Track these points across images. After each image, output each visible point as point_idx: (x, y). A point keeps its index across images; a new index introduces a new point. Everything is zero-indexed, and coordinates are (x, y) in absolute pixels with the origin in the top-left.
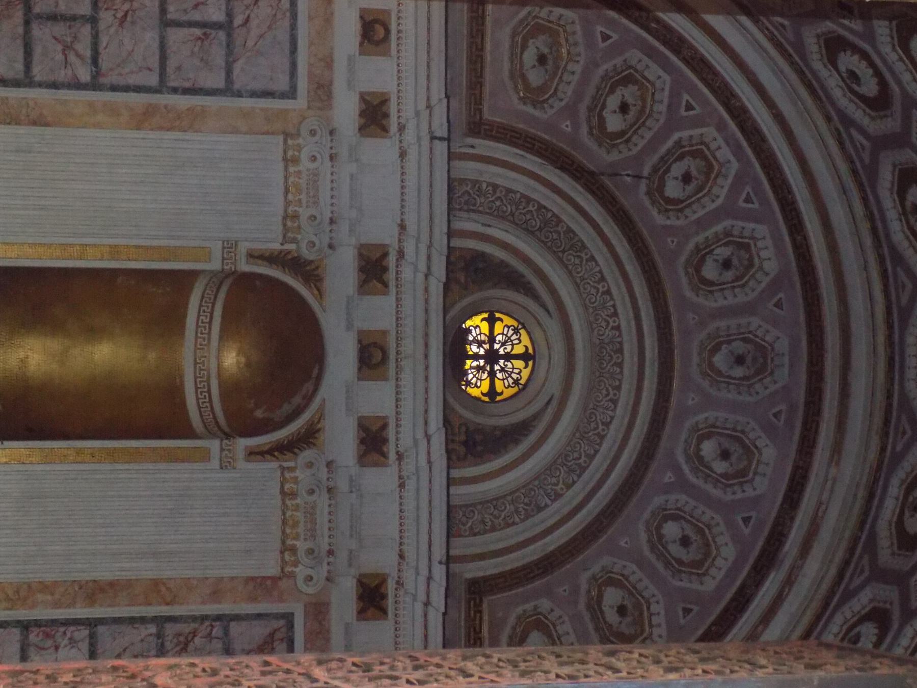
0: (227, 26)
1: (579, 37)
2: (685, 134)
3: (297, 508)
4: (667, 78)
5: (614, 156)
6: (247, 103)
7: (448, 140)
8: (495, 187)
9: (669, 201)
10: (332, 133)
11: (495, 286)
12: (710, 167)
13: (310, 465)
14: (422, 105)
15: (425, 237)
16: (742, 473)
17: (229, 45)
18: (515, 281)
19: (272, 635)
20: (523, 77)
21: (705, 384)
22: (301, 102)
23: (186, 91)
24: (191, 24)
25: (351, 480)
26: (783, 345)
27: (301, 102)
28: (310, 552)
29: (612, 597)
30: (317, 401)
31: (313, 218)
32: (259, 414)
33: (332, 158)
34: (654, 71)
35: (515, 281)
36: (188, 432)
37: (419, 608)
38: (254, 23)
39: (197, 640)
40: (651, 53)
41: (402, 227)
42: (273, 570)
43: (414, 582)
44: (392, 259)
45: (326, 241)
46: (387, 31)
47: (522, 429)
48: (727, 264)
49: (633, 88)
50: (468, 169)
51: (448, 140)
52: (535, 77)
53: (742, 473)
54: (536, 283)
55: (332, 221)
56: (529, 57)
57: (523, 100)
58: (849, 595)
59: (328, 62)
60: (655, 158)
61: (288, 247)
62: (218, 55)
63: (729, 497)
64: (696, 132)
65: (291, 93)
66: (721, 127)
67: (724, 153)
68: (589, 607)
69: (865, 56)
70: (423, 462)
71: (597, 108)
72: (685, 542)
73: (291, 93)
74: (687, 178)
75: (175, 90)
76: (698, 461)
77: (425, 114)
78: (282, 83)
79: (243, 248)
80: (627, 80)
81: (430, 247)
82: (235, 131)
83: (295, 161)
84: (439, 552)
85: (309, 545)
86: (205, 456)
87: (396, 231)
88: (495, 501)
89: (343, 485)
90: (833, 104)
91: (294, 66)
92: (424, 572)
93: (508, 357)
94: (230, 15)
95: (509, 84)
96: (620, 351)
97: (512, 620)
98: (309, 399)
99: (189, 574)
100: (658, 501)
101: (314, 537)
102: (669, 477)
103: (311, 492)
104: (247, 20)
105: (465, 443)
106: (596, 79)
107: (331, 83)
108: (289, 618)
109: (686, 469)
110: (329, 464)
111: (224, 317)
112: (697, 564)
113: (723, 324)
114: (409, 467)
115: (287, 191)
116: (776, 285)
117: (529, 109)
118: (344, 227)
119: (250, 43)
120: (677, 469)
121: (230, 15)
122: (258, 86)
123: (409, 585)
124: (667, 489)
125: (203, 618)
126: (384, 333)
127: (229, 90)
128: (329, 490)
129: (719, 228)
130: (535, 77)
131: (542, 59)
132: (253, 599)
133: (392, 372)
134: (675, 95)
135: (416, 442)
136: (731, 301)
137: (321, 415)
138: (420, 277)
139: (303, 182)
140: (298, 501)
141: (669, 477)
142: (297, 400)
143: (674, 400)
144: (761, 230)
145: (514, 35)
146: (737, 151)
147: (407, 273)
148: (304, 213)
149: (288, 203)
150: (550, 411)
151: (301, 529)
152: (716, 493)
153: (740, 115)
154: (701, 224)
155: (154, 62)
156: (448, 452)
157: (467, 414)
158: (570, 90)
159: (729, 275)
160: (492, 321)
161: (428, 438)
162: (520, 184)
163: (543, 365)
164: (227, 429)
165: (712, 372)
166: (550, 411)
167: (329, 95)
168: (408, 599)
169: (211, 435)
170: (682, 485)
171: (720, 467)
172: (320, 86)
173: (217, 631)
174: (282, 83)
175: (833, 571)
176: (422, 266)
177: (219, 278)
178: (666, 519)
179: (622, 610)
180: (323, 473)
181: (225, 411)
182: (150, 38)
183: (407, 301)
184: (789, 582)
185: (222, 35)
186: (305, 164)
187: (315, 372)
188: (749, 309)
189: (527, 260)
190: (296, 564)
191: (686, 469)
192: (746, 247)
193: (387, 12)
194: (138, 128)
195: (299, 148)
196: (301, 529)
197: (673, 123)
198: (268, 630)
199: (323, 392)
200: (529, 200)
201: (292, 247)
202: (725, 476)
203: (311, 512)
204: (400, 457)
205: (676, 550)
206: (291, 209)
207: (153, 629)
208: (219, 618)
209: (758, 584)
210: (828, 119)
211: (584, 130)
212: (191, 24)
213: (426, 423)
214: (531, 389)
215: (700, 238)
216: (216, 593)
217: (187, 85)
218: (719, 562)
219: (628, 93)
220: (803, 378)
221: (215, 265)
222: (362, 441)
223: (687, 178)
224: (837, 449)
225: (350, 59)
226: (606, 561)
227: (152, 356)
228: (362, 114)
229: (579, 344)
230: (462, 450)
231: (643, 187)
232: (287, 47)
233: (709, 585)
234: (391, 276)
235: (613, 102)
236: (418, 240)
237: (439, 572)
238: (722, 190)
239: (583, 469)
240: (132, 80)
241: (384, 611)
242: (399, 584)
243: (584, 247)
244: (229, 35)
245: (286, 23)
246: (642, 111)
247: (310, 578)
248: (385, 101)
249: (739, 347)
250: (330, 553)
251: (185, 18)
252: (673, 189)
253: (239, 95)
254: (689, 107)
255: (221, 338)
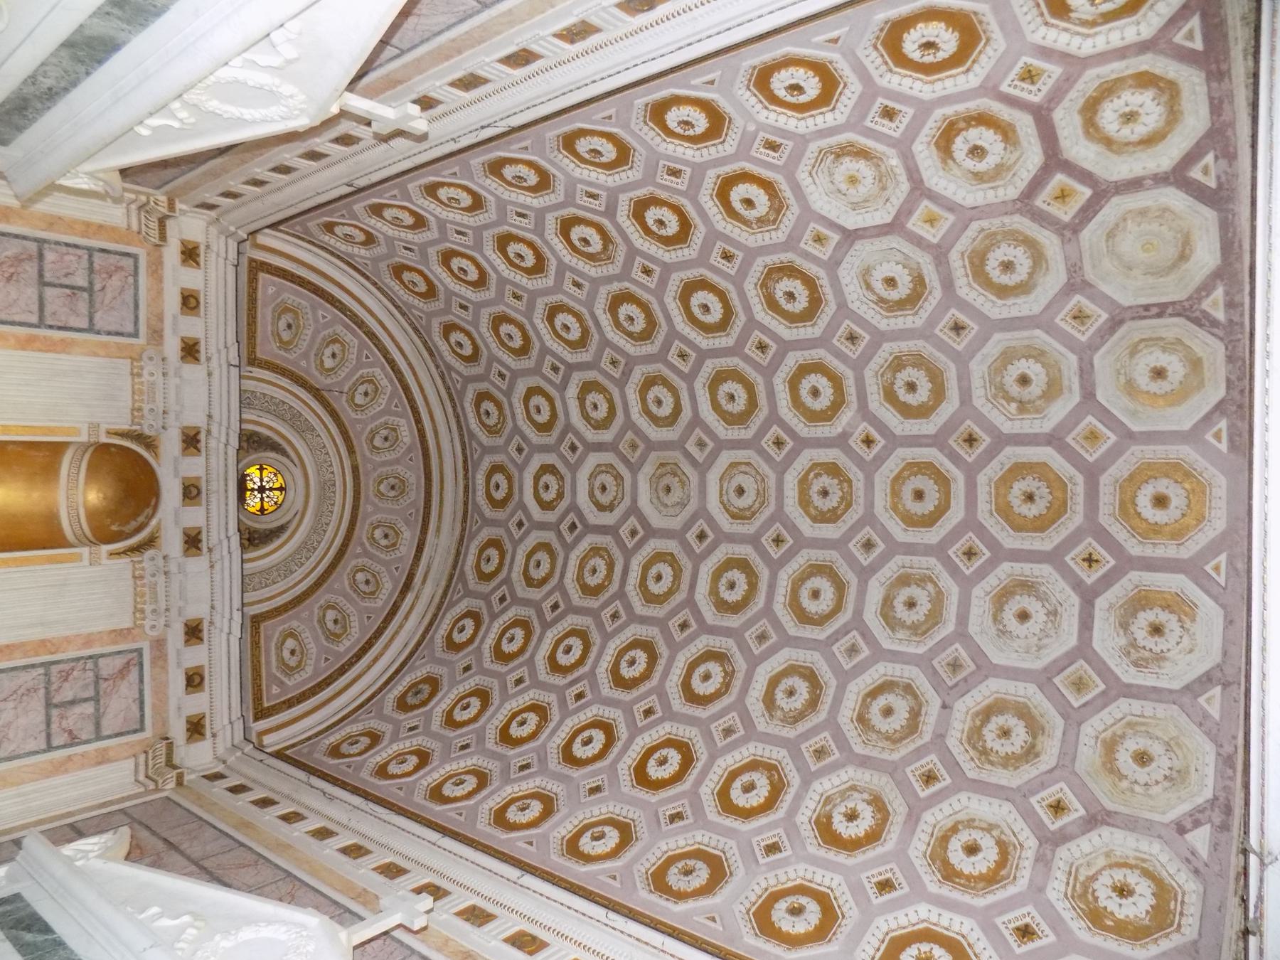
0: (90, 290)
1: (310, 316)
2: (365, 371)
3: (143, 586)
4: (356, 341)
5: (329, 381)
6: (104, 338)
7: (239, 366)
8: (265, 395)
9: (357, 405)
10: (163, 360)
11: (265, 450)
12: (377, 388)
13: (153, 559)
14: (221, 346)
15: (225, 423)
16: (394, 545)
17: (91, 303)
18: (275, 447)
19: (128, 663)
20: (278, 335)
21: (376, 501)
22: (141, 341)
23: (60, 328)
24: (62, 286)
25: (179, 565)
26: (413, 480)
27: (141, 341)
28: (154, 611)
29: (331, 615)
30: (154, 522)
31: (152, 410)
32: (114, 528)
33: (164, 374)
34: (349, 337)
35: (275, 447)
36: (63, 543)
37: (224, 637)
38: (109, 290)
39: (75, 673)
40: (347, 327)
41: (210, 416)
42: (127, 623)
43: (221, 622)
44: (202, 437)
45: (160, 424)
46: (198, 302)
47: (281, 529)
48: (386, 439)
49: (337, 345)
50: (249, 385)
51: (239, 366)
52: (286, 336)
53: (394, 545)
54: (292, 454)
55: (164, 412)
56: (282, 324)
57: (280, 348)
58: (452, 605)
59: (161, 318)
60: (351, 383)
61: (134, 428)
62: (83, 307)
63: (388, 558)
64: (370, 370)
65: (135, 335)
66: (383, 369)
67: (385, 382)
68: (319, 621)
69: (468, 334)
70: (225, 552)
71: (319, 355)
72: (367, 582)
73: (135, 335)
74: (366, 394)
75: (51, 327)
76: (372, 539)
77: (224, 352)
78: (129, 328)
79: (104, 427)
80: (335, 341)
81: (228, 428)
82: (96, 355)
83: (140, 375)
84: (237, 603)
85: (153, 607)
86: (79, 558)
87: (205, 419)
88: (267, 571)
89: (173, 568)
90: (442, 358)
91: (137, 317)
92: (227, 615)
93: (271, 489)
94: (91, 283)
95: (271, 338)
96: (334, 485)
97: (277, 635)
98: (150, 518)
99: (68, 633)
100: (354, 562)
101: (156, 602)
102: (359, 550)
103: (154, 575)
104: (103, 288)
105: (249, 540)
106: (319, 340)
107: (162, 330)
108: (139, 652)
109: (367, 545)
110: (165, 557)
111: (88, 470)
112: (373, 593)
113: (384, 469)
114: (216, 556)
115: (134, 393)
116: (409, 450)
117: (282, 353)
118: (172, 416)
119: (106, 302)
120: (362, 544)
121: (91, 283)
122: (113, 328)
123: (218, 624)
124: (358, 556)
125: (78, 659)
126: (198, 478)
127: (91, 329)
128: (166, 573)
129: (382, 420)
130: (286, 336)
131: (289, 326)
132: (115, 643)
133: (204, 502)
134: (360, 351)
135: (220, 541)
136: (389, 458)
137: (158, 528)
138: (222, 446)
139: (145, 388)
140: (145, 581)
141: (359, 550)
142: (141, 519)
143: (361, 509)
144: (403, 422)
145: (274, 311)
146: (391, 381)
147: (213, 443)
148: (146, 407)
149: (134, 401)
150: (298, 517)
151: (147, 598)
152: (383, 556)
153: (391, 362)
154: (374, 418)
155: (35, 308)
156: (242, 545)
157: (249, 523)
158: (305, 344)
159: (387, 444)
160: (261, 469)
161: (228, 538)
162: (279, 394)
163: (291, 493)
164: (92, 539)
165: (380, 495)
166: (298, 517)
167: (161, 337)
168: (217, 631)
169: (82, 544)
170: (366, 553)
171: (384, 542)
172: (155, 331)
173: (90, 665)
174: (129, 328)
175: (440, 591)
176: (223, 439)
177: (85, 447)
178: (357, 571)
179: (336, 622)
180: (160, 562)
181: (92, 529)
182: (31, 292)
183: (213, 460)
184: (417, 597)
185: (86, 295)
186: (146, 377)
187: (153, 503)
188: (397, 461)
189: (289, 442)
190: (144, 619)
191: (367, 545)
192: (395, 430)
193: (198, 292)
194: (23, 349)
195: (142, 368)
196: (147, 598)
197: (360, 365)
198: (125, 661)
199: (159, 515)
200: (284, 403)
201: (137, 427)
202: (387, 547)
203: (153, 587)
204: (210, 550)
205: (363, 587)
206: (137, 405)
207: (41, 671)
208: (90, 657)
209: (403, 600)
210: (437, 367)
211: (313, 365)
212: (62, 286)
213: (227, 530)
214: (285, 506)
215: (373, 425)
216: (89, 641)
217: (60, 324)
218: (384, 591)
219: (336, 348)
220: (423, 495)
221: (84, 438)
222: (186, 542)
223: (366, 394)
224: (438, 530)
225: (174, 317)
226: (328, 596)
227: (36, 495)
228: (183, 349)
229: (312, 482)
230: (246, 543)
231: (344, 398)
232: (132, 305)
233: (380, 603)
234: (202, 445)
235: (328, 352)
236: (220, 424)
237: (237, 616)
238: (383, 401)
239: (315, 549)
240: (17, 318)
241: (201, 640)
242: (211, 623)
243: (314, 429)
244: (91, 295)
245: (132, 291)
246: (342, 359)
247: (153, 627)
248: (196, 343)
249: (392, 481)
250: (167, 610)
251: (57, 282)
252: (359, 399)
253: (98, 333)
254: (367, 357)
255: (86, 483)
